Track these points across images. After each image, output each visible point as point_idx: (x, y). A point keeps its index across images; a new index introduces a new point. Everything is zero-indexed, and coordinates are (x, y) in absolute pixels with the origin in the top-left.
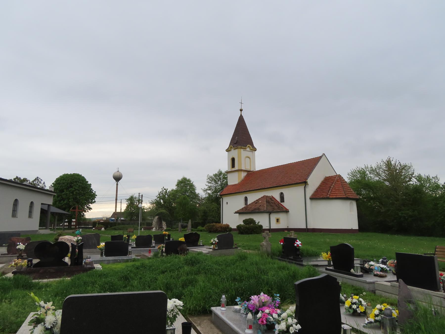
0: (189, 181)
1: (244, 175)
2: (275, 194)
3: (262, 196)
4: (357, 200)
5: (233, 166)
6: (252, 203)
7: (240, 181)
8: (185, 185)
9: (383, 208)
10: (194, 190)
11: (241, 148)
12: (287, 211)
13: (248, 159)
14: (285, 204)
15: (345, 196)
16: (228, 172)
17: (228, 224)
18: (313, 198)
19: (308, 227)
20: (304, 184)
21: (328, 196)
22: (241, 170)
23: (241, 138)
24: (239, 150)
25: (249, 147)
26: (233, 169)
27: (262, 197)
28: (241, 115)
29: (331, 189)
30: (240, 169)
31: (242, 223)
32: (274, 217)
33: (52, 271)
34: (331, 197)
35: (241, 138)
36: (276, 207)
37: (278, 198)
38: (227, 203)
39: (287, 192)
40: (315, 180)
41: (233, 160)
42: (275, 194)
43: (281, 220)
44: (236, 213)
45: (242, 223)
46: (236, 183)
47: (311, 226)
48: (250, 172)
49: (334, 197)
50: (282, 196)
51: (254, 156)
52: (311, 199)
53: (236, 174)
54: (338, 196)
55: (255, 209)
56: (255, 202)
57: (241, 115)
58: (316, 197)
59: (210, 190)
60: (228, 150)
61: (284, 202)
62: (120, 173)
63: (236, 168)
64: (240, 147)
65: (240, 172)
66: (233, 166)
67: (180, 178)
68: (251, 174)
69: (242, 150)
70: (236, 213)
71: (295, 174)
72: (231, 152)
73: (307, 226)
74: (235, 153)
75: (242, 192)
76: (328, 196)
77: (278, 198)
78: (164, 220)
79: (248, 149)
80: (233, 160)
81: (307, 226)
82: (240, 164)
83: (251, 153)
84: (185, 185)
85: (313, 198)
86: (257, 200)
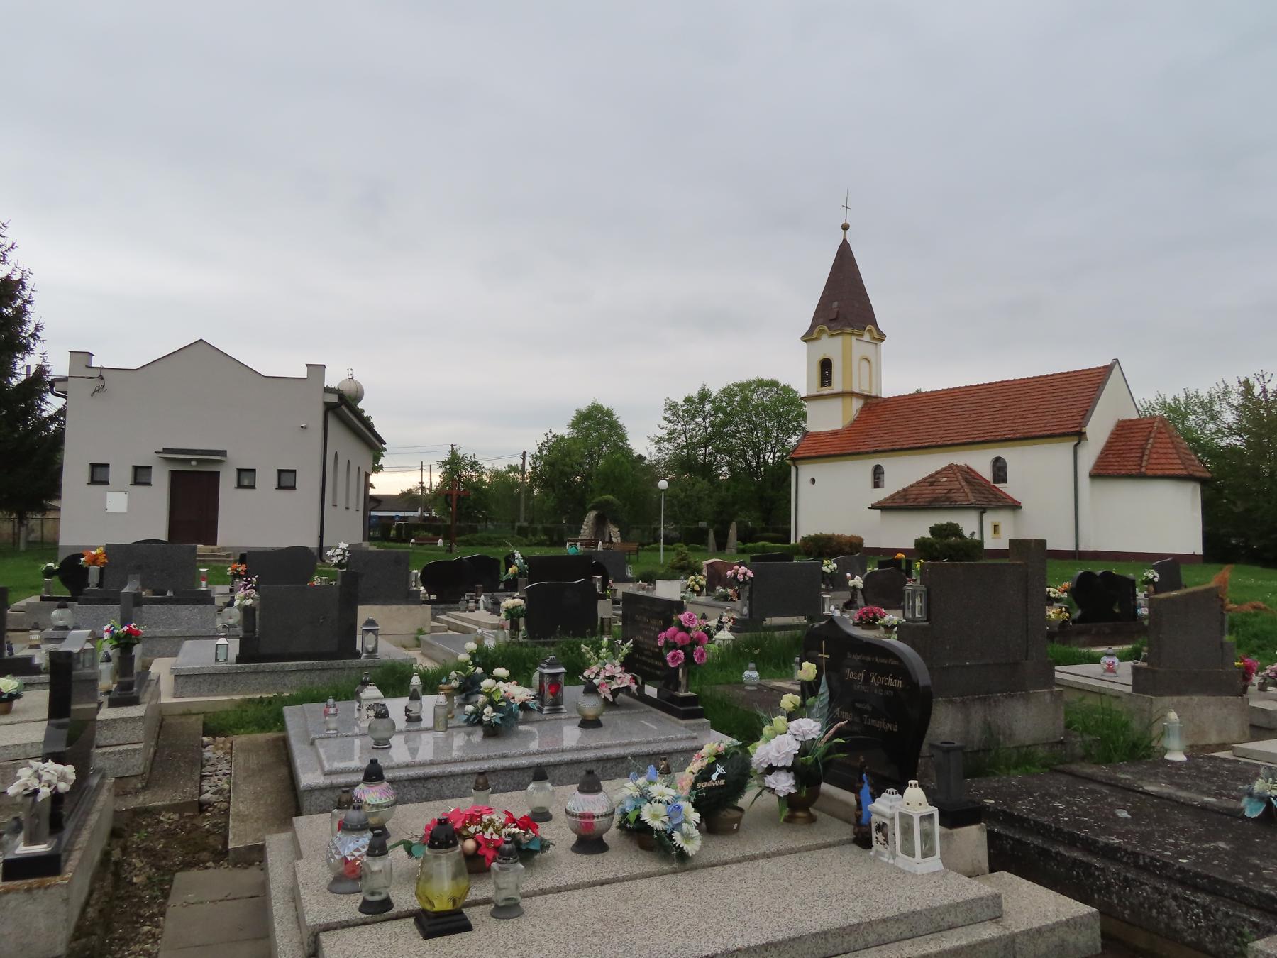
0: (609, 413)
1: (857, 405)
2: (980, 462)
3: (945, 465)
4: (1203, 482)
5: (826, 379)
6: (918, 483)
7: (847, 422)
8: (597, 423)
9: (1239, 503)
10: (623, 438)
11: (852, 334)
12: (1015, 506)
13: (865, 363)
14: (1009, 489)
15: (1185, 472)
16: (809, 398)
17: (857, 535)
18: (1100, 473)
19: (1082, 548)
20: (1077, 438)
21: (1143, 470)
22: (852, 394)
23: (845, 305)
24: (847, 337)
25: (870, 330)
26: (826, 391)
27: (944, 469)
28: (845, 240)
29: (1137, 452)
30: (848, 389)
31: (928, 535)
32: (990, 518)
33: (1107, 631)
34: (1149, 473)
35: (845, 305)
36: (990, 495)
37: (986, 472)
38: (813, 481)
39: (1014, 457)
40: (1099, 430)
41: (826, 365)
42: (980, 462)
43: (1002, 529)
44: (873, 507)
45: (928, 535)
46: (838, 426)
47: (1088, 545)
48: (875, 401)
49: (1159, 473)
50: (999, 469)
51: (878, 354)
52: (1094, 476)
53: (837, 404)
54: (1167, 472)
55: (936, 499)
56: (924, 480)
57: (845, 240)
58: (1105, 471)
59: (669, 440)
60: (808, 338)
61: (1005, 481)
62: (356, 382)
63: (837, 385)
64: (849, 330)
65: (848, 400)
66: (826, 379)
67: (584, 406)
68: (873, 404)
69: (854, 338)
70: (873, 507)
71: (1049, 408)
72: (817, 343)
73: (1077, 545)
74: (831, 346)
75: (867, 453)
76: (1143, 470)
77: (986, 472)
78: (616, 522)
79: (867, 337)
80: (826, 365)
81: (1077, 545)
82: (847, 376)
83: (872, 347)
84: (597, 423)
85: (1100, 473)
86: (931, 476)
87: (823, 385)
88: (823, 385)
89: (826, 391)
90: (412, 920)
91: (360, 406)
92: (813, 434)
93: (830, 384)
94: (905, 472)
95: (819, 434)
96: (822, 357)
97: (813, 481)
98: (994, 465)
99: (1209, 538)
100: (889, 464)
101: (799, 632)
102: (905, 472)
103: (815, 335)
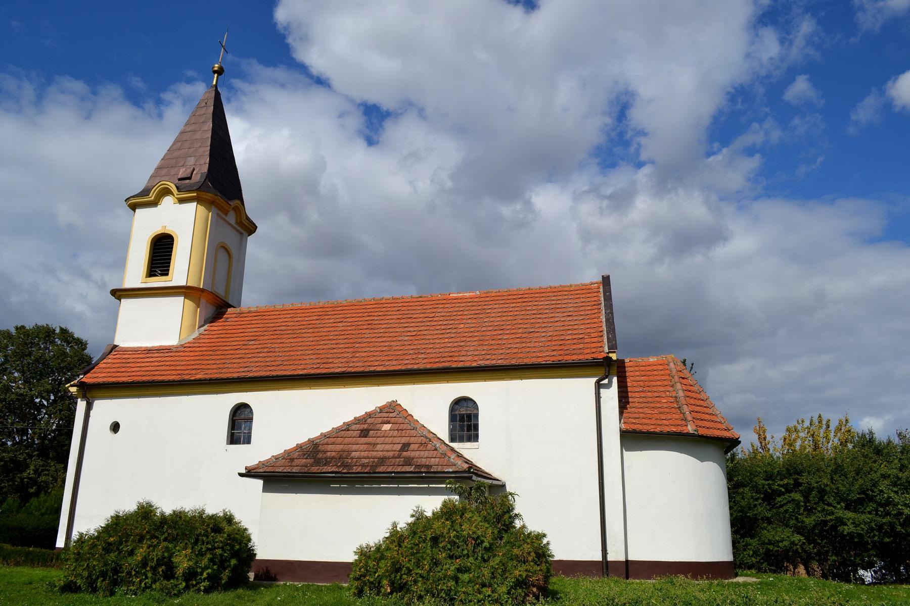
38: (115, 427)
42: (428, 405)
50: (464, 420)
70: (250, 473)
87: (151, 273)
88: (151, 273)
89: (158, 282)
90: (602, 390)
91: (429, 514)
92: (126, 350)
93: (165, 272)
94: (293, 418)
95: (136, 351)
96: (157, 230)
97: (115, 427)
98: (453, 418)
99: (742, 525)
100: (259, 400)
101: (459, 462)
102: (293, 418)
103: (152, 197)
